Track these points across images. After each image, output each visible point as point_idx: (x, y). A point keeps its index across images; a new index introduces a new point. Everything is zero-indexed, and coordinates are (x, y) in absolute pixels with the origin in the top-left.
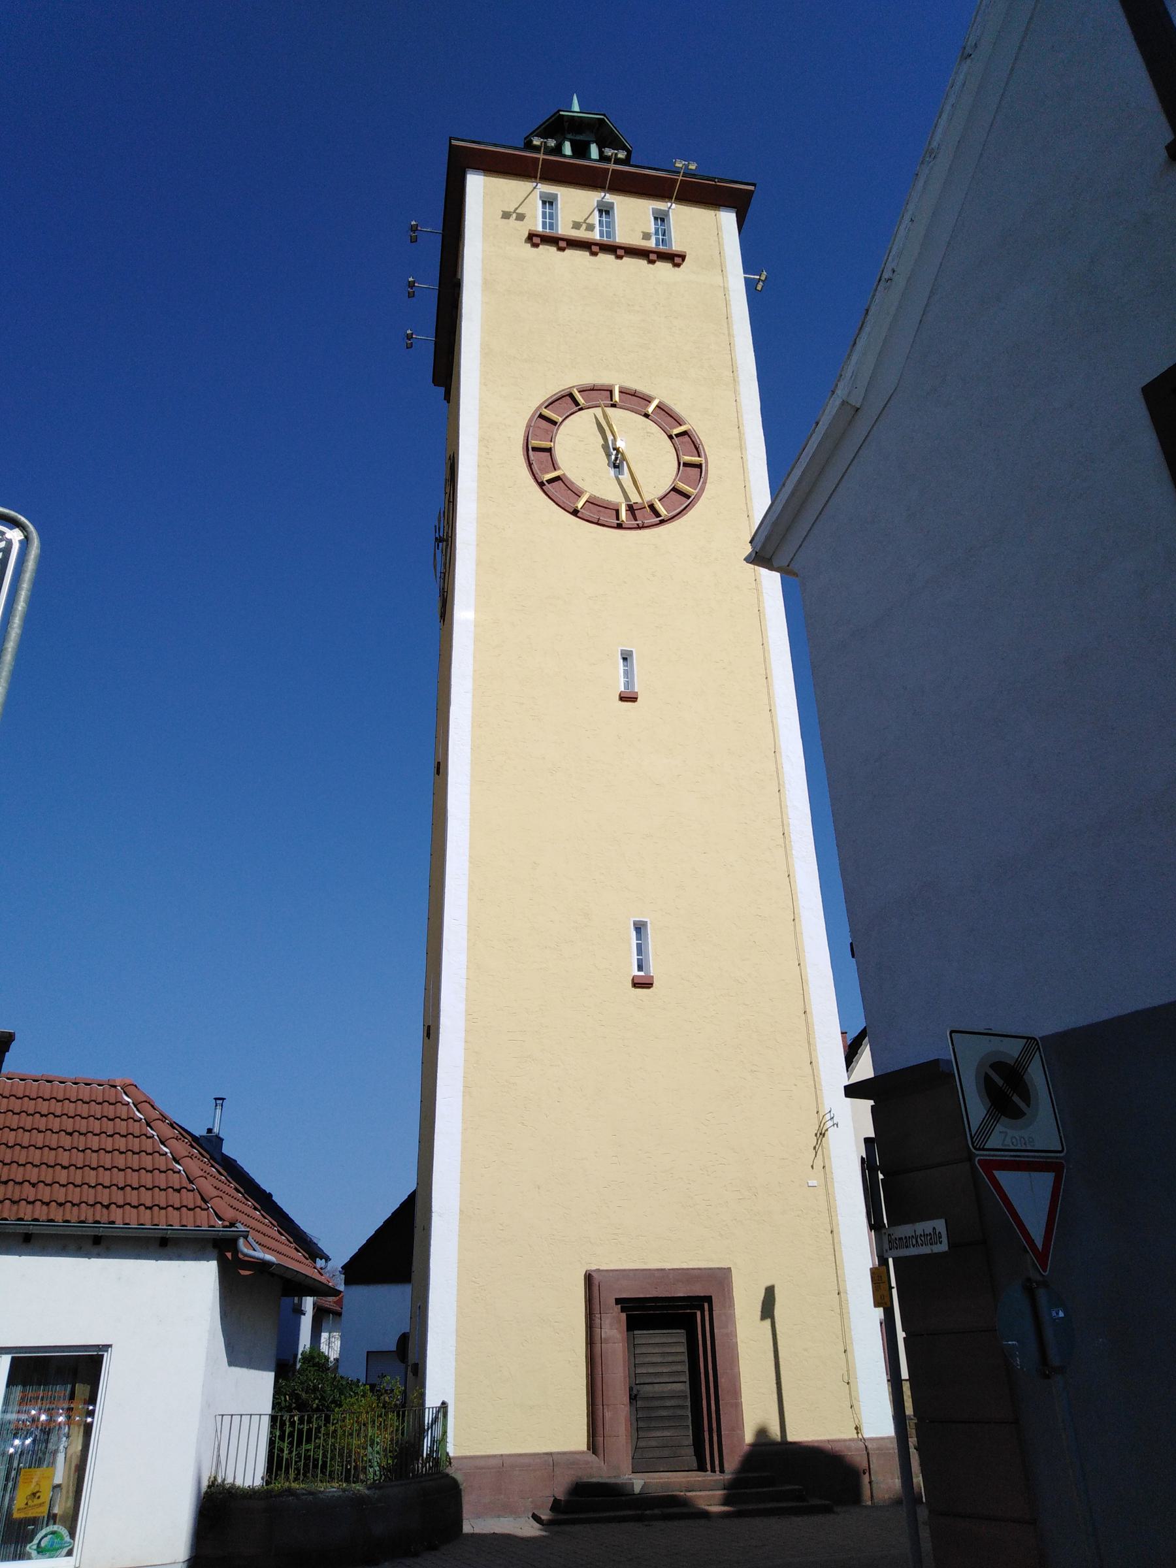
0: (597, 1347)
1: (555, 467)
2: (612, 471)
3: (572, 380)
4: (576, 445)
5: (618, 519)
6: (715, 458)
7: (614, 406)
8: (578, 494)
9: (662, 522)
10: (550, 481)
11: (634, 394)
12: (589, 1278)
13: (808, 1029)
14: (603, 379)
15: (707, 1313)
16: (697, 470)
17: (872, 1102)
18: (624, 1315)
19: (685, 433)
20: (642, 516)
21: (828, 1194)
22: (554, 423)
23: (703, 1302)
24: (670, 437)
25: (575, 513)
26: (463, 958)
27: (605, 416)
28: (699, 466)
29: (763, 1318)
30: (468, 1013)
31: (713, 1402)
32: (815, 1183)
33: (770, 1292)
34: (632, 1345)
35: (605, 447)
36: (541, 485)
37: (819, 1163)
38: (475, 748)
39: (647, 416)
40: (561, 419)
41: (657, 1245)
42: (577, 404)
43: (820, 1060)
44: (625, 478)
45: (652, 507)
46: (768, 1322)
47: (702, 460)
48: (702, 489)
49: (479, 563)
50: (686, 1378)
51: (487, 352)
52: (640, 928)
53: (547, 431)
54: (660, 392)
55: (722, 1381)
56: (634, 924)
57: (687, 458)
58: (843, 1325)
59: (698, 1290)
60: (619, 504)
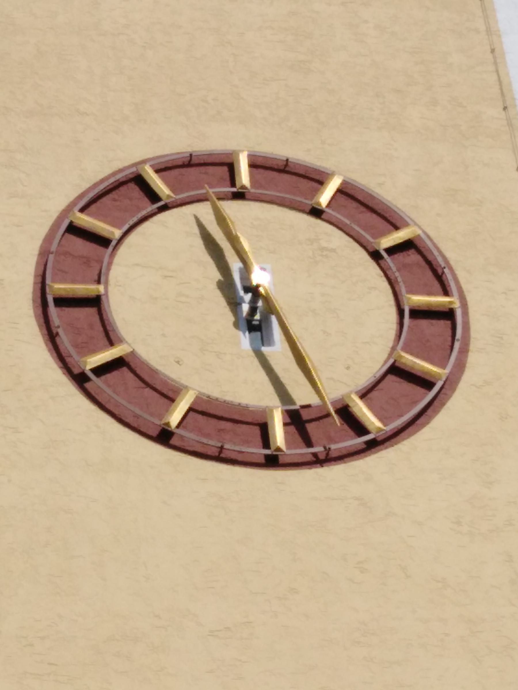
1: (110, 338)
2: (245, 340)
3: (137, 147)
4: (159, 291)
7: (240, 196)
8: (169, 395)
9: (373, 445)
10: (101, 370)
11: (285, 168)
14: (211, 141)
16: (443, 325)
20: (323, 435)
22: (103, 241)
24: (376, 256)
25: (164, 437)
27: (221, 220)
28: (448, 315)
35: (226, 286)
36: (80, 379)
39: (316, 212)
40: (117, 233)
42: (152, 196)
44: (277, 350)
45: (345, 412)
48: (460, 367)
53: (87, 261)
54: (343, 163)
57: (419, 299)
60: (266, 412)
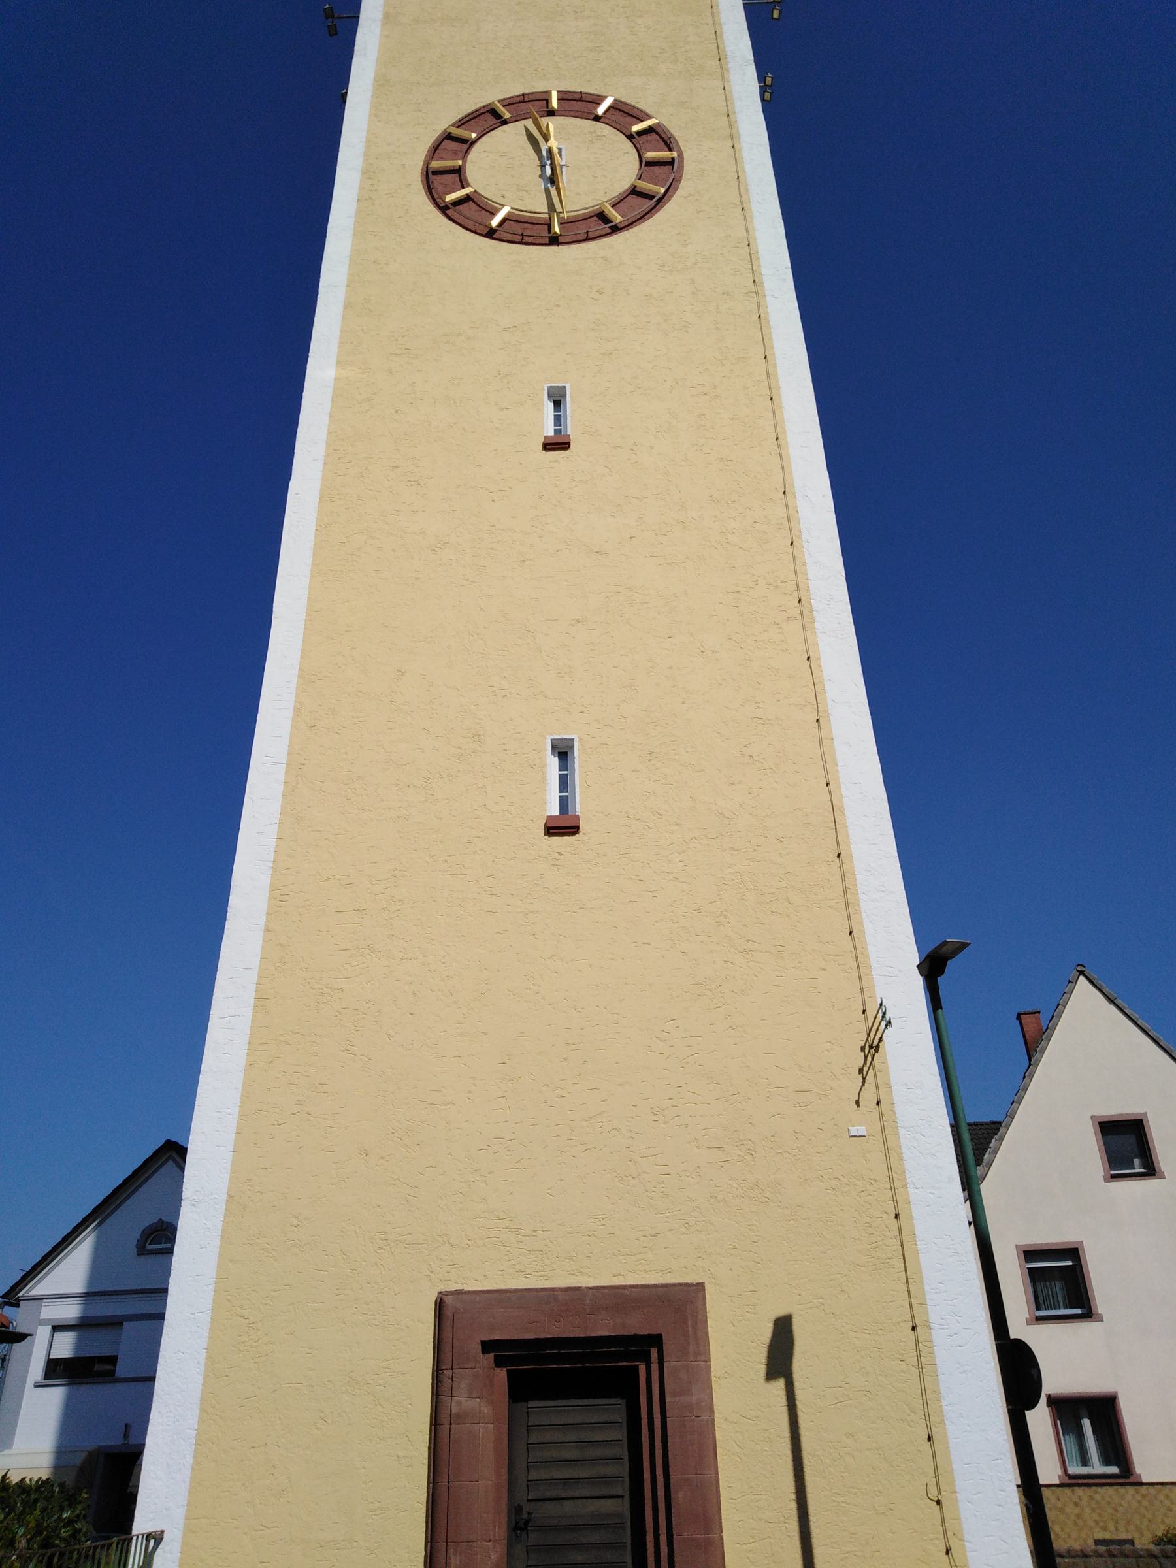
0: (445, 1428)
5: (550, 232)
6: (695, 153)
12: (440, 1305)
13: (844, 881)
15: (655, 1367)
17: (1027, 1412)
18: (502, 1374)
19: (650, 130)
21: (886, 1149)
23: (646, 1345)
24: (630, 137)
26: (275, 808)
29: (770, 1376)
30: (274, 888)
31: (663, 1538)
32: (862, 1130)
33: (783, 1329)
34: (516, 1432)
36: (444, 209)
37: (869, 1096)
38: (322, 528)
41: (567, 1247)
43: (868, 927)
46: (780, 1383)
47: (675, 154)
49: (348, 306)
50: (623, 1488)
51: (382, 84)
52: (563, 752)
55: (680, 1497)
56: (554, 747)
58: (923, 1388)
59: (635, 1324)
